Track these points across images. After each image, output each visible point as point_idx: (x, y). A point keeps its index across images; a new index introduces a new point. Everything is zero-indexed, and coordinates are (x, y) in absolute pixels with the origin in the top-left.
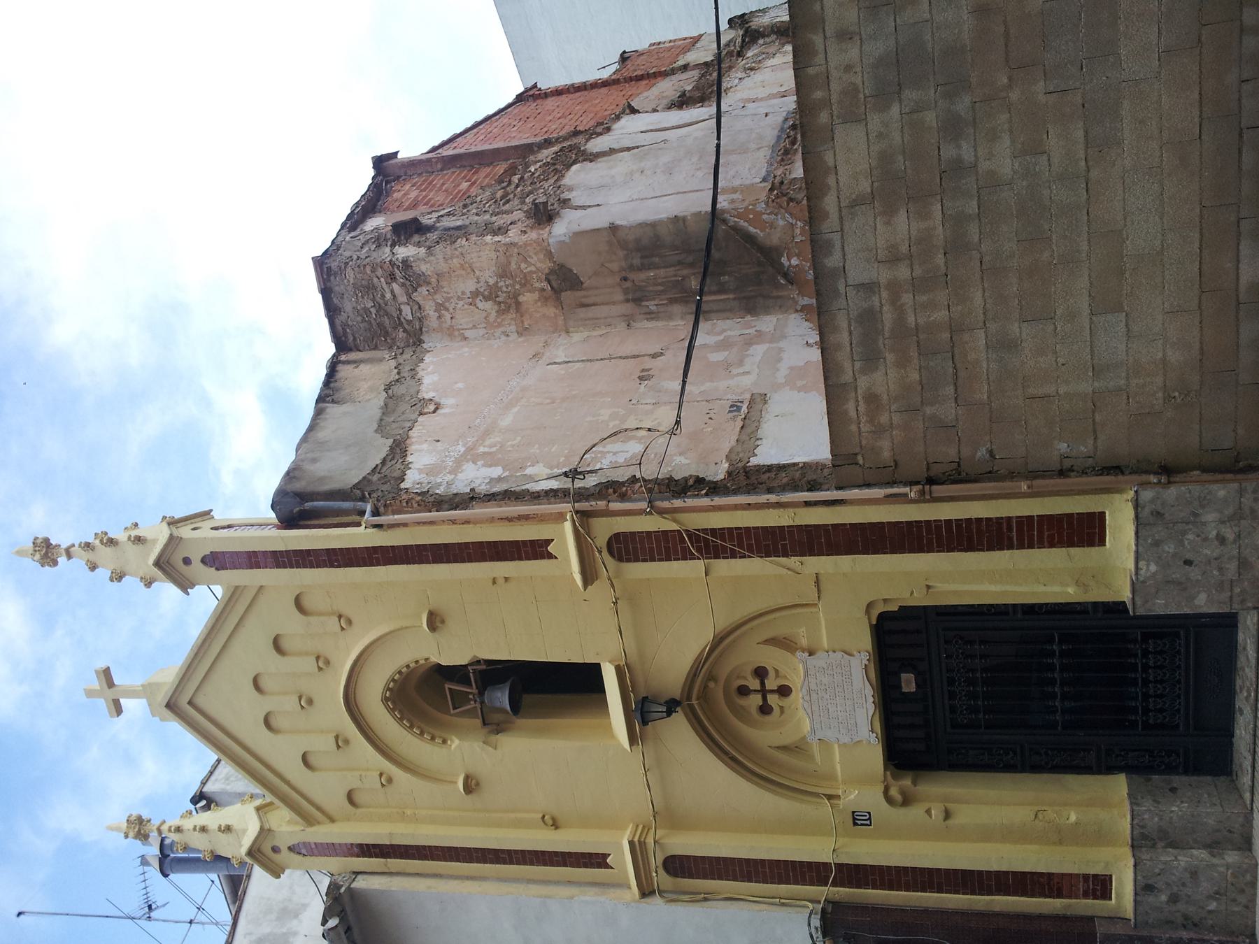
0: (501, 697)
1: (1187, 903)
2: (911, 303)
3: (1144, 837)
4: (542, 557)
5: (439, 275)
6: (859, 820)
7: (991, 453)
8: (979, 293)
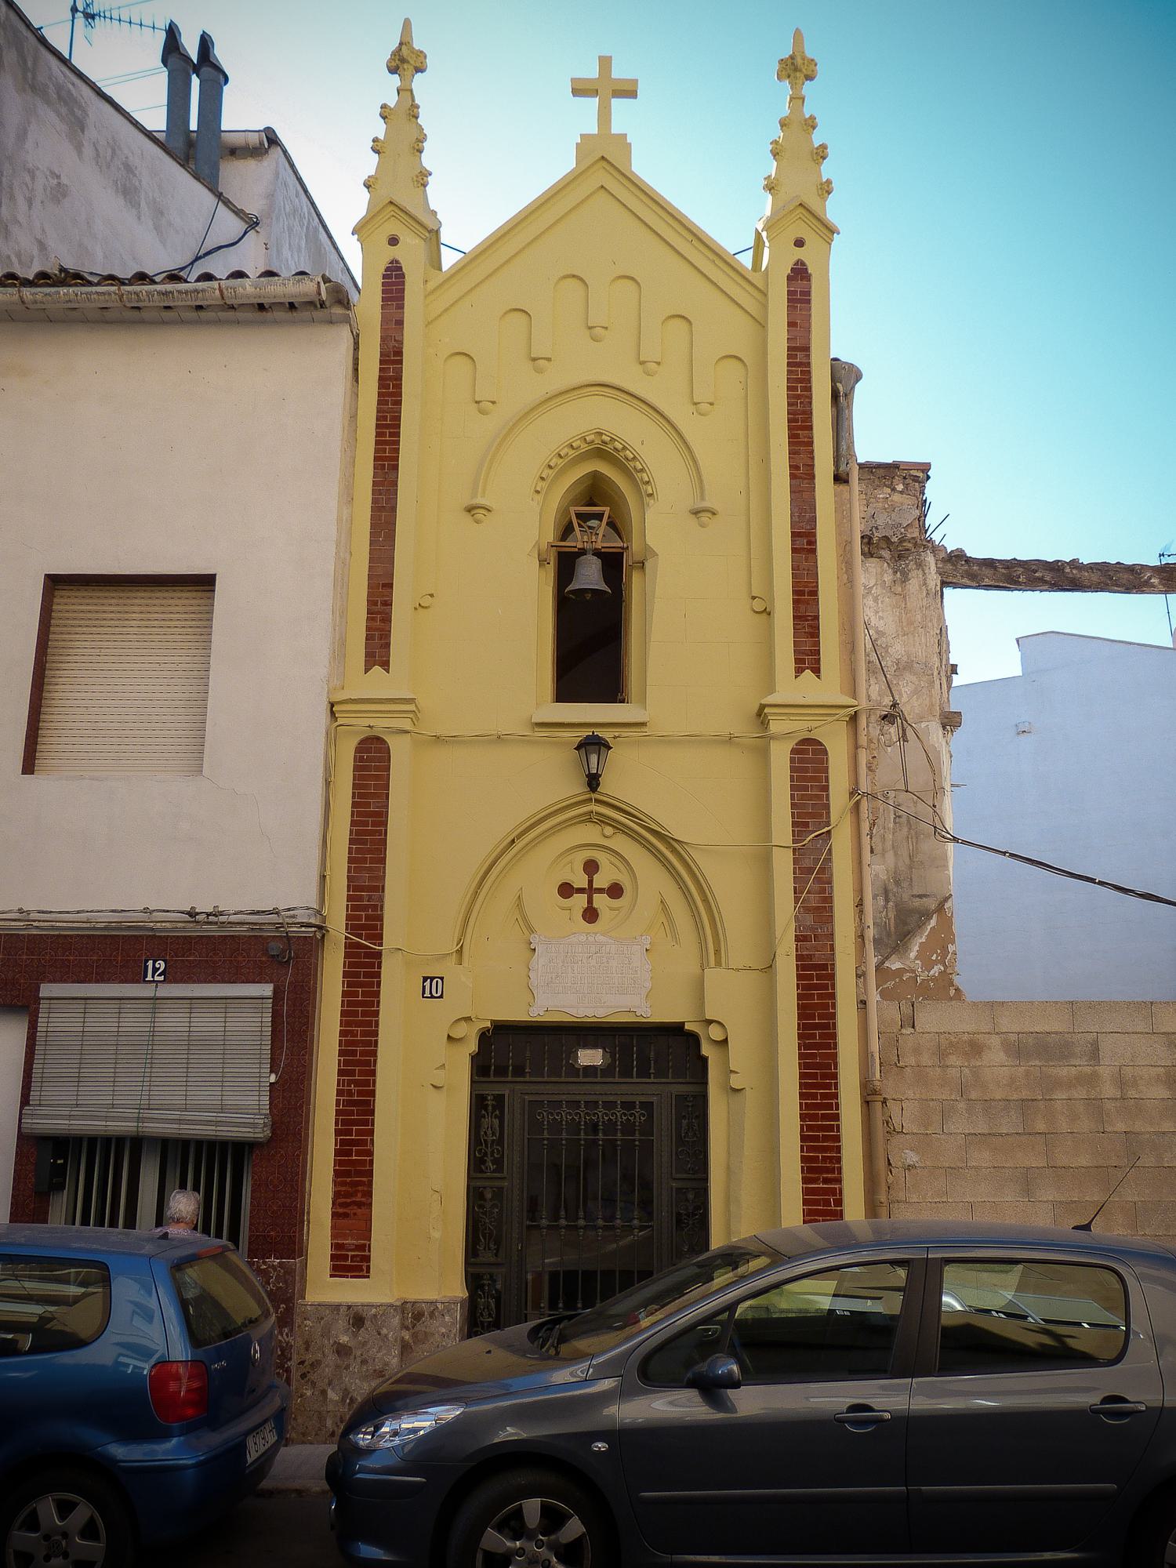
0: (590, 576)
1: (338, 1366)
2: (1076, 1096)
3: (418, 1316)
4: (797, 661)
5: (904, 597)
6: (431, 986)
7: (909, 1167)
8: (1085, 1164)
